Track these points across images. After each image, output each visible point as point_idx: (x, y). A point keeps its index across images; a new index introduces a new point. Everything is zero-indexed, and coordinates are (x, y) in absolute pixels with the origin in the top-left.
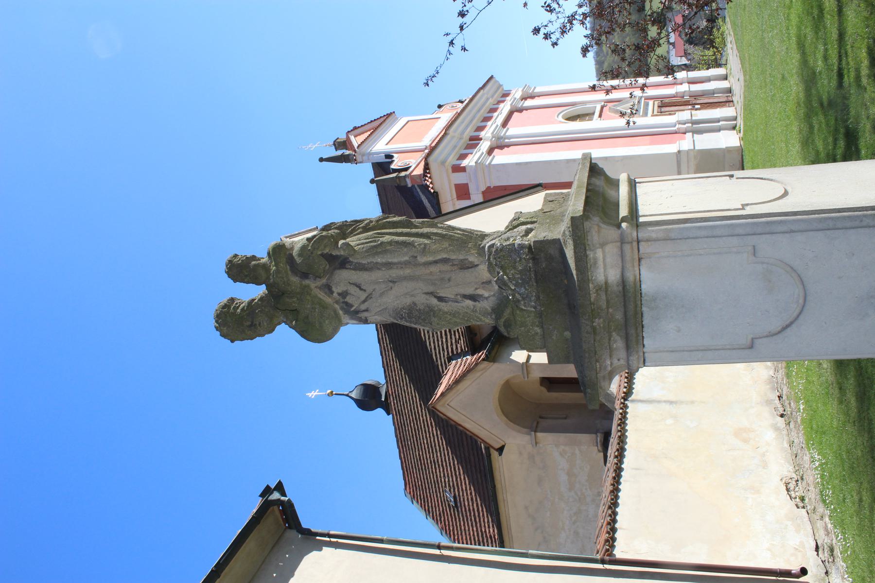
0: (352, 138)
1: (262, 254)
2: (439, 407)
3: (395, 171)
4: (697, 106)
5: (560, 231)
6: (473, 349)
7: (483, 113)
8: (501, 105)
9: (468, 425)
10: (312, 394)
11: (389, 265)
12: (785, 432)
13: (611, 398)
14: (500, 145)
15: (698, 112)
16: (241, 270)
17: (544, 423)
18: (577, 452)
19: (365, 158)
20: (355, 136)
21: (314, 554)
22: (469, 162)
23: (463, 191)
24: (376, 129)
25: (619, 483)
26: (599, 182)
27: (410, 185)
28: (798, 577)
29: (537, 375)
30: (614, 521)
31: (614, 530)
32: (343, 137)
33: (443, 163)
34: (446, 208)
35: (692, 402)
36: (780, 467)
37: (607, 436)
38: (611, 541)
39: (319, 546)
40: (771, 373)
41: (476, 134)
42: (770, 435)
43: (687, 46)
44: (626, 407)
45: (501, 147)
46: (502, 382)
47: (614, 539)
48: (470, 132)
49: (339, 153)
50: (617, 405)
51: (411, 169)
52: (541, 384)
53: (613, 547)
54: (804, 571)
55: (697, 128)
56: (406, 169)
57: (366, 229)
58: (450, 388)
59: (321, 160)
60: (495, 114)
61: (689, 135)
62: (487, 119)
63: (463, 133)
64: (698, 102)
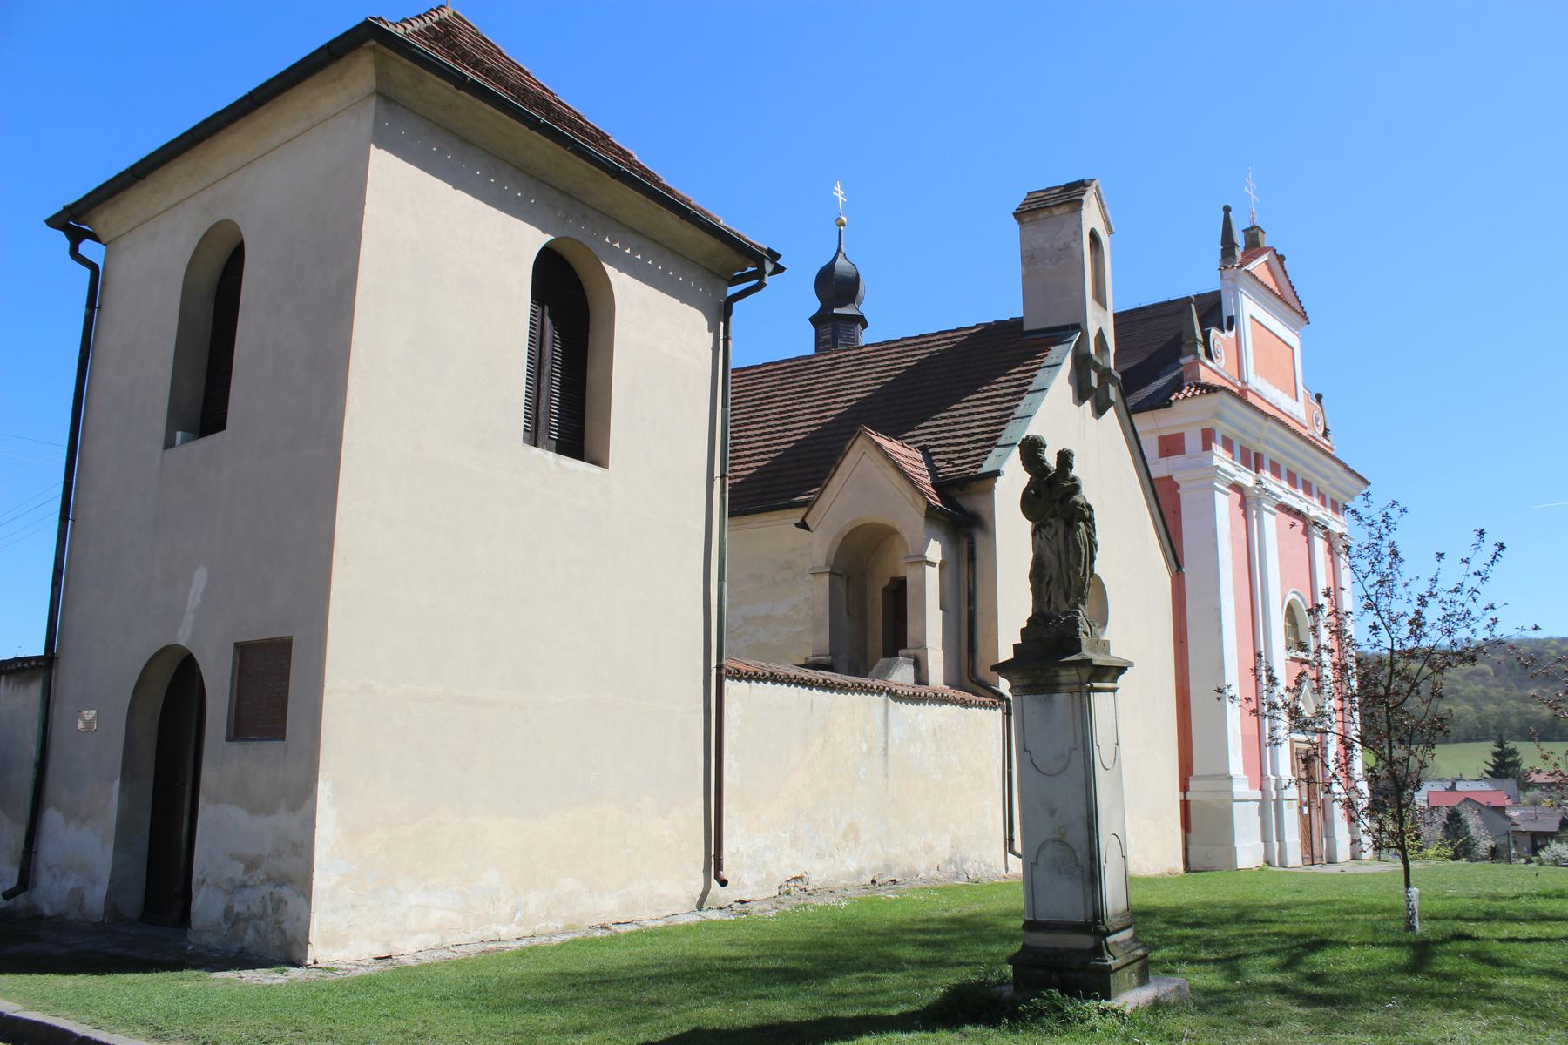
0: (1265, 258)
1: (1075, 472)
2: (860, 441)
3: (1206, 335)
4: (1306, 810)
5: (1087, 653)
6: (941, 486)
7: (1303, 473)
8: (1316, 501)
9: (836, 481)
10: (839, 192)
11: (1067, 552)
12: (856, 883)
13: (885, 673)
14: (1246, 501)
15: (1296, 810)
16: (1065, 458)
17: (841, 583)
18: (799, 628)
19: (1229, 283)
20: (1267, 262)
21: (705, 323)
22: (1220, 456)
23: (1172, 445)
24: (1282, 298)
25: (797, 684)
26: (1114, 673)
27: (1182, 361)
28: (717, 877)
29: (910, 575)
30: (758, 680)
31: (749, 679)
32: (1266, 241)
33: (1218, 415)
34: (1143, 421)
35: (886, 776)
36: (819, 872)
37: (829, 668)
38: (739, 676)
39: (713, 328)
40: (922, 875)
41: (1267, 463)
42: (852, 865)
43: (1445, 812)
44: (880, 694)
45: (1243, 504)
46: (898, 528)
47: (739, 679)
48: (1269, 453)
49: (1239, 239)
50: (877, 683)
51: (1208, 363)
52: (893, 580)
53: (733, 678)
54: (724, 883)
55: (1269, 808)
56: (1209, 355)
57: (1089, 535)
58: (887, 456)
59: (1227, 209)
60: (1300, 493)
61: (1258, 795)
62: (1292, 479)
63: (1267, 442)
64: (1314, 812)
